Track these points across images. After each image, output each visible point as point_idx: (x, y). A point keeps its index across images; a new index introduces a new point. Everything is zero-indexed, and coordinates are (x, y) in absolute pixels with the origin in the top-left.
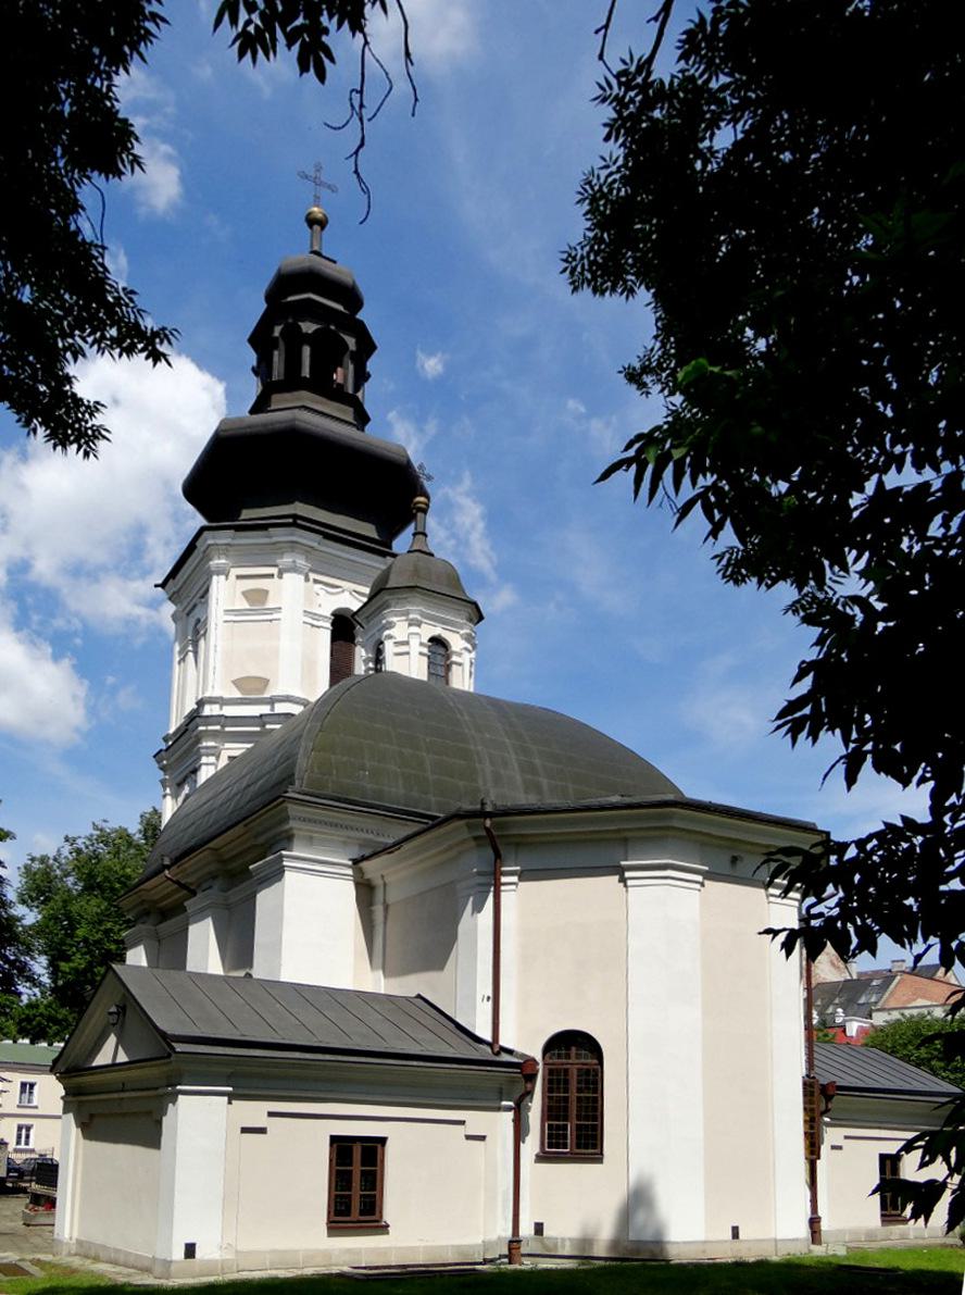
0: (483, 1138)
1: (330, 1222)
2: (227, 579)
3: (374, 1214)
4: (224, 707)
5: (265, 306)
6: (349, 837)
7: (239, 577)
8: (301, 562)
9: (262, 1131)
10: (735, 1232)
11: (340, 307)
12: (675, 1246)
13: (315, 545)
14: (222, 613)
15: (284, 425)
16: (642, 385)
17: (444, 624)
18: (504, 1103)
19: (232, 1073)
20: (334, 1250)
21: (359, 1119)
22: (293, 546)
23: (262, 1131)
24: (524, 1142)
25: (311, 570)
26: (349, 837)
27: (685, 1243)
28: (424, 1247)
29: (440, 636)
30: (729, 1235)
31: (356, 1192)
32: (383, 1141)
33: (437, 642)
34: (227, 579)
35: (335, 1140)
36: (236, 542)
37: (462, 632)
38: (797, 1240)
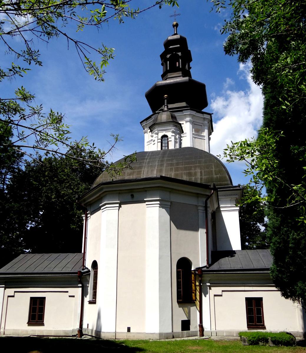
0: (74, 296)
1: (248, 325)
3: (42, 320)
6: (232, 198)
9: (221, 296)
10: (129, 329)
12: (104, 333)
13: (194, 114)
15: (163, 84)
17: (165, 131)
18: (79, 285)
19: (210, 279)
20: (29, 330)
21: (38, 292)
23: (221, 296)
24: (86, 297)
26: (232, 198)
27: (107, 332)
28: (54, 330)
29: (164, 134)
30: (126, 330)
31: (37, 313)
32: (45, 298)
35: (32, 298)
36: (147, 123)
38: (154, 333)
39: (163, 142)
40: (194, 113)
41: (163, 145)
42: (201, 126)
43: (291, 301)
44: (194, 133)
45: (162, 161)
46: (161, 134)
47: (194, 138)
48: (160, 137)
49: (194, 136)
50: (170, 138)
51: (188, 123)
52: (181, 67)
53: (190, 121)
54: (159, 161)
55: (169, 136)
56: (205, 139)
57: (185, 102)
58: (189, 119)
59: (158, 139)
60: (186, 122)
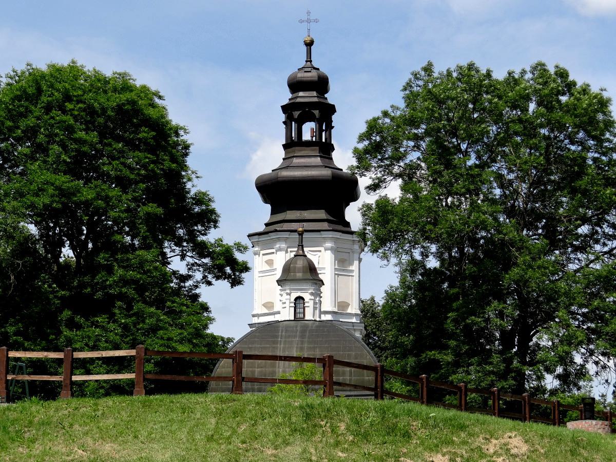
2: (259, 256)
4: (260, 318)
5: (351, 203)
7: (263, 255)
8: (284, 245)
11: (324, 124)
13: (288, 236)
14: (258, 273)
16: (405, 89)
22: (279, 239)
25: (288, 247)
33: (299, 299)
34: (259, 256)
37: (310, 292)
39: (298, 306)
40: (338, 235)
41: (298, 310)
42: (348, 254)
43: (208, 304)
44: (336, 267)
45: (302, 342)
46: (295, 295)
47: (336, 276)
48: (293, 300)
49: (336, 273)
50: (308, 302)
51: (329, 252)
52: (324, 140)
53: (331, 249)
54: (297, 347)
55: (306, 300)
56: (353, 276)
57: (314, 122)
58: (330, 245)
59: (290, 303)
60: (326, 250)
